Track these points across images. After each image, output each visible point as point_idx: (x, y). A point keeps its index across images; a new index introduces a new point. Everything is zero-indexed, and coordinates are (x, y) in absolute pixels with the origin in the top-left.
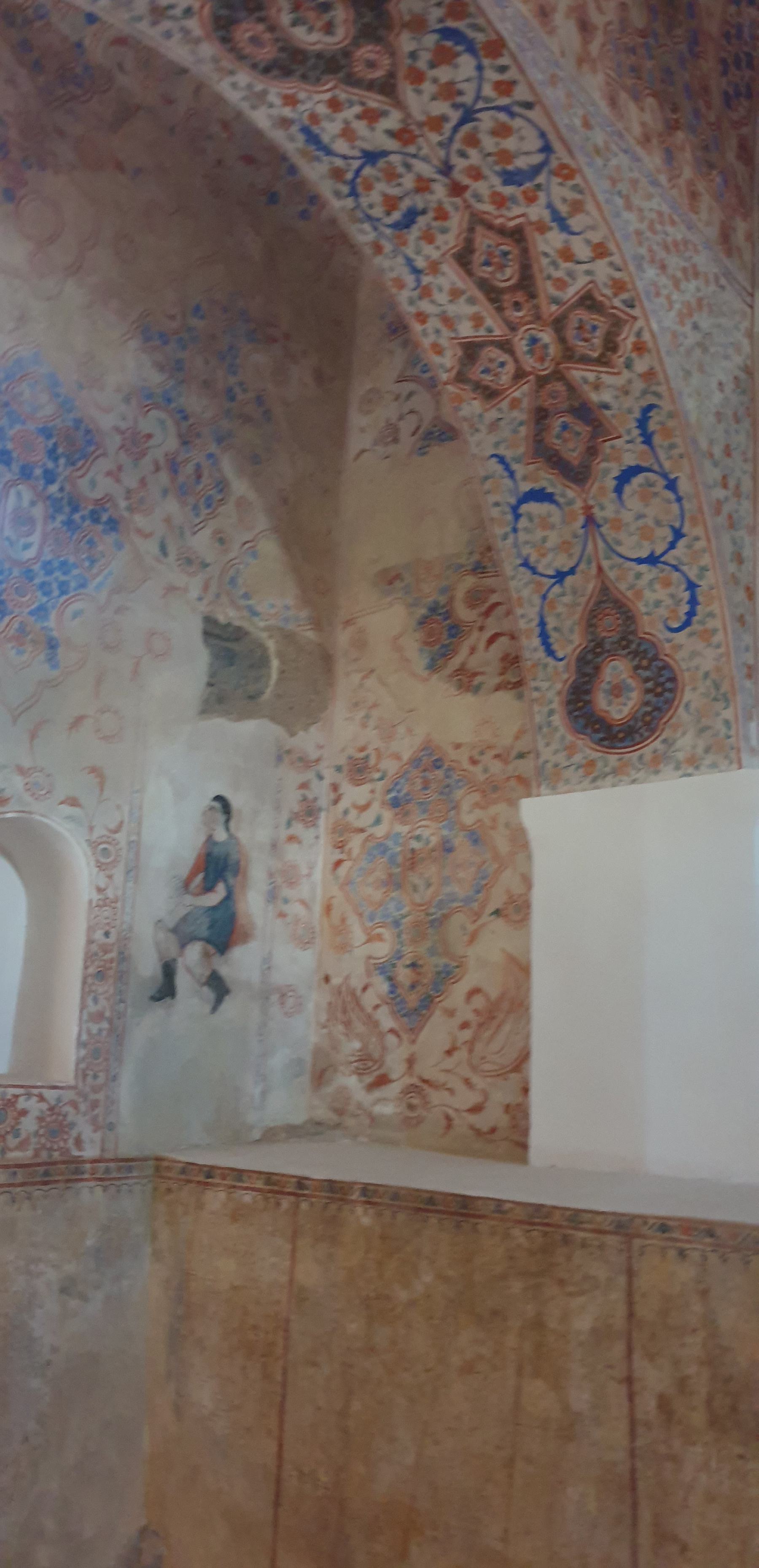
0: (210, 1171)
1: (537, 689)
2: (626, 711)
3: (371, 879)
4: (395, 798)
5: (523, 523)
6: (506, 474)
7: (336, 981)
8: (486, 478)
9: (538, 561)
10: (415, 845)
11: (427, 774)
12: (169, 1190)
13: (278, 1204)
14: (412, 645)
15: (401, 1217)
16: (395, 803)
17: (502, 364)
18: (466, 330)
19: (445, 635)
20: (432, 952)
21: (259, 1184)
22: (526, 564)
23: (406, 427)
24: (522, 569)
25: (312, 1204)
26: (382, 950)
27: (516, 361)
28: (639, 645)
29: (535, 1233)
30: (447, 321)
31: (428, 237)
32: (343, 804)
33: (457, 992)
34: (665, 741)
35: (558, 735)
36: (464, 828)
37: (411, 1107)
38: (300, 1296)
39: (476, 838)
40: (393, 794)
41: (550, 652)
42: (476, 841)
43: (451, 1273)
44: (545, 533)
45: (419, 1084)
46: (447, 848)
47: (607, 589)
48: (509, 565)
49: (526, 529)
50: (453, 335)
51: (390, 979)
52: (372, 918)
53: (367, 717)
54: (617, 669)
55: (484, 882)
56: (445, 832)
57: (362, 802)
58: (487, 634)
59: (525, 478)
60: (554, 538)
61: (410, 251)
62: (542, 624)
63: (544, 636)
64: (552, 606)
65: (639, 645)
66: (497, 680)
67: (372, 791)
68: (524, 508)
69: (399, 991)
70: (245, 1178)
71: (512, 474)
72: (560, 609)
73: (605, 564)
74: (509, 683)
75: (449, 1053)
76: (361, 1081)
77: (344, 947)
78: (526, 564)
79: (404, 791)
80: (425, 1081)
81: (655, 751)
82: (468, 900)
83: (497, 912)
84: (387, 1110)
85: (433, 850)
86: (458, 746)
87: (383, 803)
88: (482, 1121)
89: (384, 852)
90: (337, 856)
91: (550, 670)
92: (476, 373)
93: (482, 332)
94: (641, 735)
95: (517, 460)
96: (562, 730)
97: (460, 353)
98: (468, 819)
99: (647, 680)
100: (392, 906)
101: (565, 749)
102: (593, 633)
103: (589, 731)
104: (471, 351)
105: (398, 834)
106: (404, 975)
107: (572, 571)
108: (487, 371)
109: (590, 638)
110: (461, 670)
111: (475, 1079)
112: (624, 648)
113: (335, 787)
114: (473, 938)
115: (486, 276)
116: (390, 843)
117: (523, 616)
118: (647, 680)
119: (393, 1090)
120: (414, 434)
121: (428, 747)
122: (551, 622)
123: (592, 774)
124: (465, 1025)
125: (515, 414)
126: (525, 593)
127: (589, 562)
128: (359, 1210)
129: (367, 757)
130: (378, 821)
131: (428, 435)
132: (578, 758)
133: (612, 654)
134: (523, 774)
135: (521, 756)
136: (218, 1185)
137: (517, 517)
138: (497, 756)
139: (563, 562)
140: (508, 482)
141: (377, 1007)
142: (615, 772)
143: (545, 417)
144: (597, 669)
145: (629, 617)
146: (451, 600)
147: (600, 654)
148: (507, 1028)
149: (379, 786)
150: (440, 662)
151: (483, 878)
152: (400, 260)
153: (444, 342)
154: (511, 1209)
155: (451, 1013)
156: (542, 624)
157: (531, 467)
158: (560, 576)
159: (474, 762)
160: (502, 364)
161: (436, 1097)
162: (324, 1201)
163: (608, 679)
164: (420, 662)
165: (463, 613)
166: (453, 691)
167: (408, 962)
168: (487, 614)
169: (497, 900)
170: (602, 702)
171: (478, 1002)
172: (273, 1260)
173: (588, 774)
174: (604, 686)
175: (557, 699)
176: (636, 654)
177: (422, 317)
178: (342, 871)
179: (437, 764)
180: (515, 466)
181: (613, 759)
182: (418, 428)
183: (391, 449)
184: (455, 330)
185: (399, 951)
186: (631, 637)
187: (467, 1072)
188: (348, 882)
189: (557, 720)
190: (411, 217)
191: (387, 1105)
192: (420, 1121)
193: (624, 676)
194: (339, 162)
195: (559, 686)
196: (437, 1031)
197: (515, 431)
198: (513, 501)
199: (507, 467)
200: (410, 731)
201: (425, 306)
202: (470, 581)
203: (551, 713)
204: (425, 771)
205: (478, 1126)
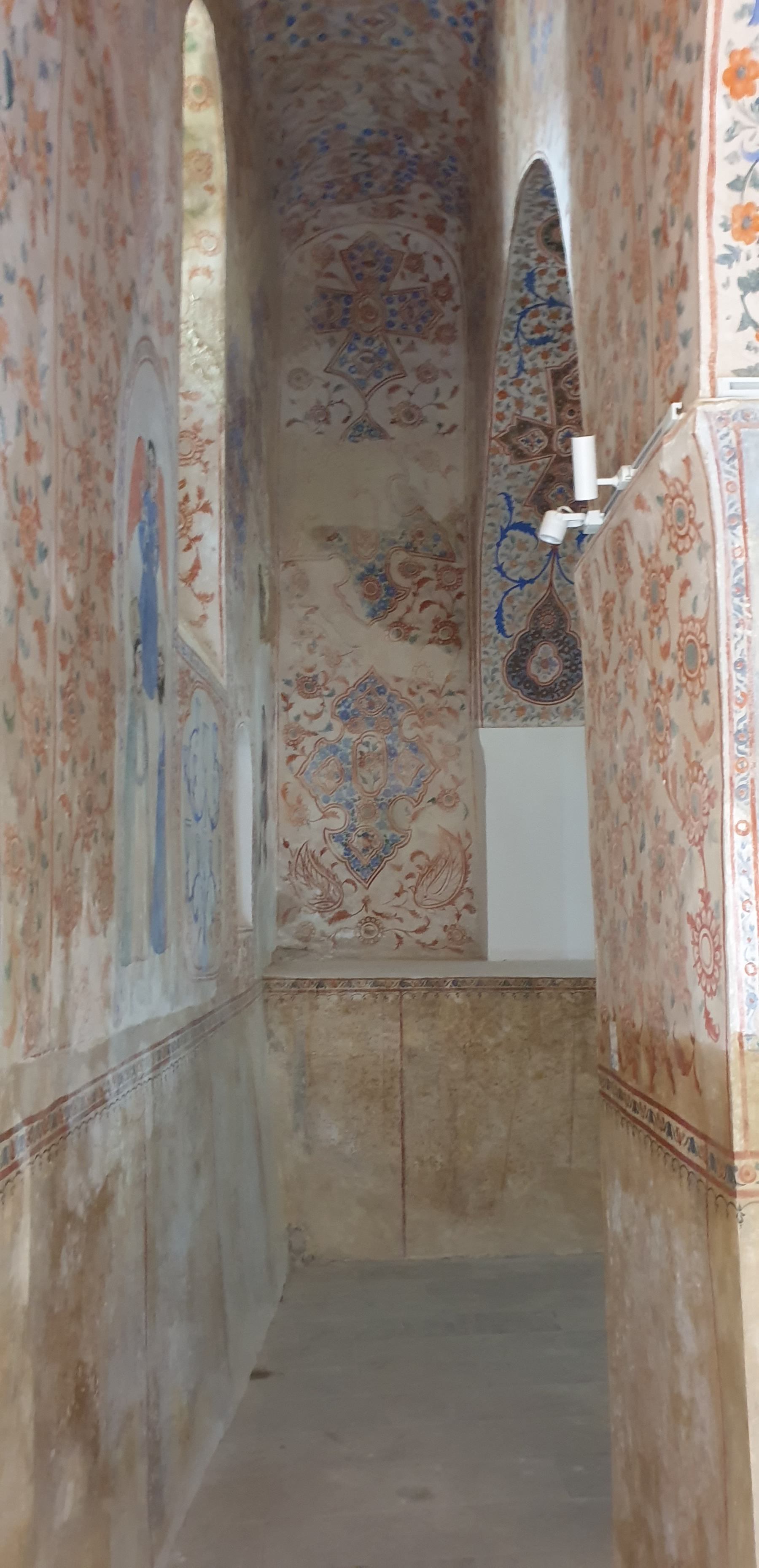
0: (320, 983)
1: (486, 653)
2: (549, 678)
3: (324, 771)
4: (345, 712)
5: (506, 541)
6: (507, 507)
7: (295, 846)
8: (491, 506)
9: (508, 569)
10: (365, 750)
11: (372, 697)
12: (282, 1000)
13: (385, 998)
14: (353, 594)
15: (484, 995)
16: (344, 716)
17: (539, 441)
18: (528, 413)
19: (384, 592)
20: (381, 826)
21: (368, 987)
22: (499, 568)
23: (337, 414)
24: (496, 571)
25: (414, 996)
26: (338, 823)
27: (550, 442)
28: (565, 637)
29: (577, 994)
30: (520, 403)
31: (545, 355)
32: (293, 713)
33: (404, 854)
34: (574, 701)
35: (498, 687)
36: (404, 740)
37: (367, 932)
38: (410, 1054)
39: (414, 747)
40: (343, 709)
41: (501, 629)
42: (416, 750)
43: (524, 1023)
44: (520, 552)
45: (374, 916)
46: (391, 753)
47: (553, 597)
48: (486, 567)
49: (507, 547)
50: (518, 413)
51: (345, 845)
52: (326, 801)
53: (314, 644)
54: (546, 650)
55: (422, 779)
56: (390, 742)
57: (314, 712)
58: (420, 601)
59: (519, 514)
60: (525, 557)
61: (526, 357)
62: (500, 610)
63: (499, 618)
64: (510, 600)
65: (565, 637)
66: (430, 636)
67: (322, 704)
68: (510, 532)
69: (353, 853)
70: (353, 983)
71: (511, 509)
72: (516, 603)
73: (555, 583)
74: (439, 640)
75: (398, 895)
76: (323, 917)
77: (302, 821)
78: (499, 568)
79: (352, 708)
80: (377, 914)
81: (568, 706)
82: (410, 792)
83: (433, 800)
84: (349, 935)
85: (379, 754)
86: (398, 680)
87: (333, 715)
88: (427, 938)
89: (335, 753)
90: (291, 751)
91: (498, 642)
92: (519, 441)
93: (539, 418)
94: (559, 695)
95: (519, 501)
96: (502, 683)
97: (515, 424)
98: (409, 734)
99: (567, 660)
100: (344, 792)
101: (504, 696)
102: (536, 624)
103: (522, 686)
104: (523, 426)
105: (348, 740)
106: (357, 842)
107: (531, 581)
108: (527, 441)
109: (532, 626)
110: (399, 623)
111: (418, 911)
112: (554, 638)
113: (285, 698)
114: (415, 817)
115: (565, 389)
116: (341, 746)
117: (486, 602)
118: (567, 660)
119: (353, 921)
120: (345, 421)
121: (371, 676)
122: (507, 610)
123: (523, 717)
124: (410, 876)
125: (533, 473)
126: (493, 587)
127: (545, 578)
128: (453, 994)
129: (316, 676)
130: (329, 728)
131: (358, 427)
132: (512, 703)
133: (545, 640)
134: (481, 713)
135: (451, 693)
136: (330, 991)
137: (503, 536)
138: (431, 691)
139: (526, 574)
140: (506, 513)
141: (333, 865)
142: (539, 716)
143: (551, 481)
144: (533, 648)
145: (562, 619)
146: (388, 565)
147: (538, 638)
148: (443, 876)
149: (328, 701)
150: (381, 613)
151: (422, 776)
152: (517, 358)
153: (508, 414)
154: (560, 983)
155: (399, 868)
156: (500, 610)
157: (526, 509)
158: (522, 583)
159: (412, 693)
160: (539, 441)
161: (387, 924)
162: (423, 992)
163: (539, 655)
164: (362, 610)
165: (398, 578)
166: (393, 637)
167: (360, 833)
168: (420, 583)
169: (433, 791)
170: (533, 669)
171: (420, 860)
172: (386, 1034)
173: (519, 716)
174: (536, 659)
175: (501, 663)
176: (561, 643)
177: (503, 395)
178: (297, 763)
179: (381, 691)
180: (514, 504)
181: (538, 708)
182: (348, 418)
183: (323, 427)
184: (521, 411)
185: (352, 825)
186: (561, 631)
187: (412, 906)
188: (302, 772)
189: (498, 676)
190: (544, 340)
191: (348, 932)
192: (376, 941)
193: (551, 655)
194: (531, 297)
195: (504, 654)
196: (386, 882)
197: (527, 484)
198: (505, 526)
199: (509, 503)
200: (355, 661)
201: (512, 390)
202: (403, 556)
203: (495, 670)
204: (369, 694)
205: (422, 941)
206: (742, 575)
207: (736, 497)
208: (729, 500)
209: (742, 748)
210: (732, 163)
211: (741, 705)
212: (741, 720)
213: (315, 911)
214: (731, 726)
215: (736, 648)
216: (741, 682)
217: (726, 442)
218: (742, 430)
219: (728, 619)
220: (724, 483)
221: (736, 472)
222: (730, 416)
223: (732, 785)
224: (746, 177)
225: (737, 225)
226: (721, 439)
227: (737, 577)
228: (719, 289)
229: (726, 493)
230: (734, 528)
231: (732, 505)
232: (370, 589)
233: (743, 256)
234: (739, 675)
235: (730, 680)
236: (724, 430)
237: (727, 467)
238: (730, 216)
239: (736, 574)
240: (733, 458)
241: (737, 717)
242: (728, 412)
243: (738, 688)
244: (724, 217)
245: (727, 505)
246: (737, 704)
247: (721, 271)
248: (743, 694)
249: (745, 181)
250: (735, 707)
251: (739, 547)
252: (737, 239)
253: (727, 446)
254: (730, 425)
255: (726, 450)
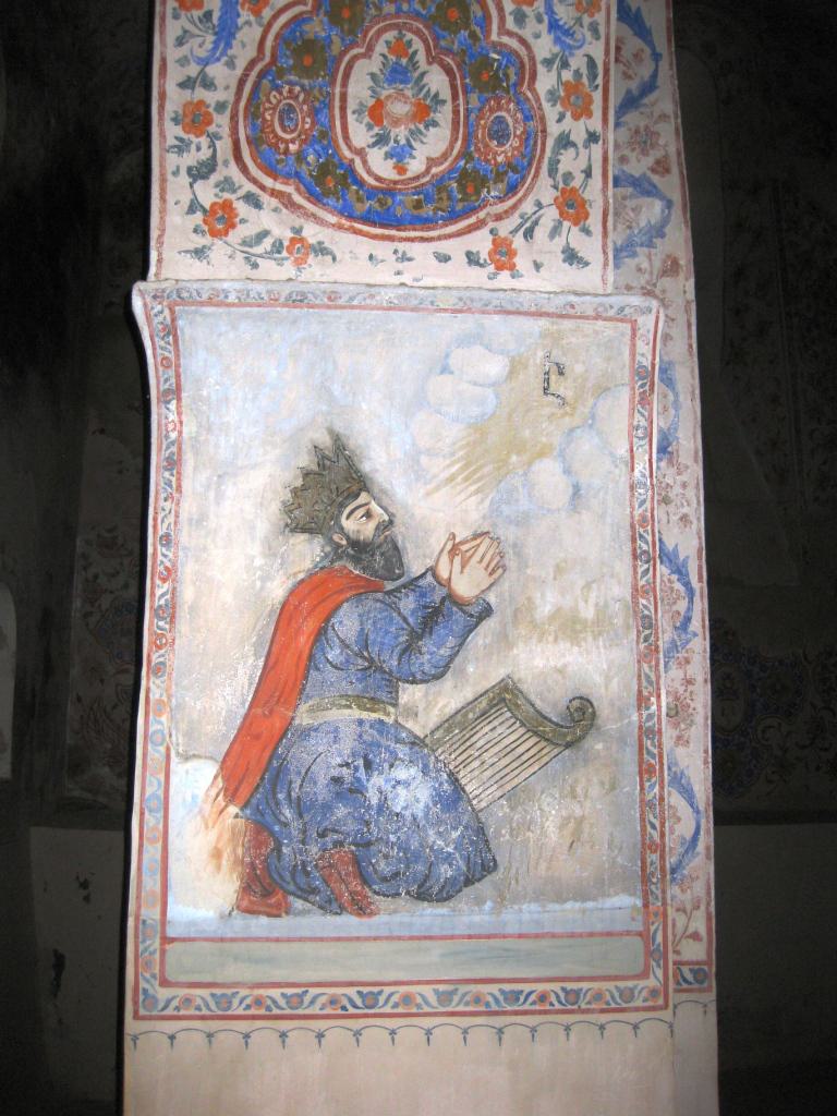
206: (174, 449)
207: (171, 372)
208: (164, 374)
209: (161, 623)
210: (182, 66)
211: (164, 580)
212: (162, 595)
213: (104, 765)
214: (152, 601)
215: (163, 521)
216: (165, 556)
217: (160, 318)
218: (177, 308)
219: (157, 493)
220: (159, 359)
221: (171, 348)
222: (165, 295)
223: (149, 662)
224: (197, 78)
225: (187, 120)
226: (156, 315)
227: (169, 451)
228: (170, 177)
229: (161, 369)
230: (169, 402)
231: (166, 380)
232: (304, 488)
233: (193, 147)
234: (164, 550)
235: (155, 554)
236: (159, 308)
237: (162, 343)
238: (181, 112)
239: (168, 448)
240: (168, 334)
241: (159, 592)
242: (163, 291)
243: (162, 562)
244: (176, 112)
245: (162, 380)
246: (160, 578)
247: (173, 160)
248: (166, 568)
249: (195, 82)
250: (158, 582)
251: (173, 421)
252: (188, 133)
253: (162, 323)
254: (165, 303)
255: (160, 327)
